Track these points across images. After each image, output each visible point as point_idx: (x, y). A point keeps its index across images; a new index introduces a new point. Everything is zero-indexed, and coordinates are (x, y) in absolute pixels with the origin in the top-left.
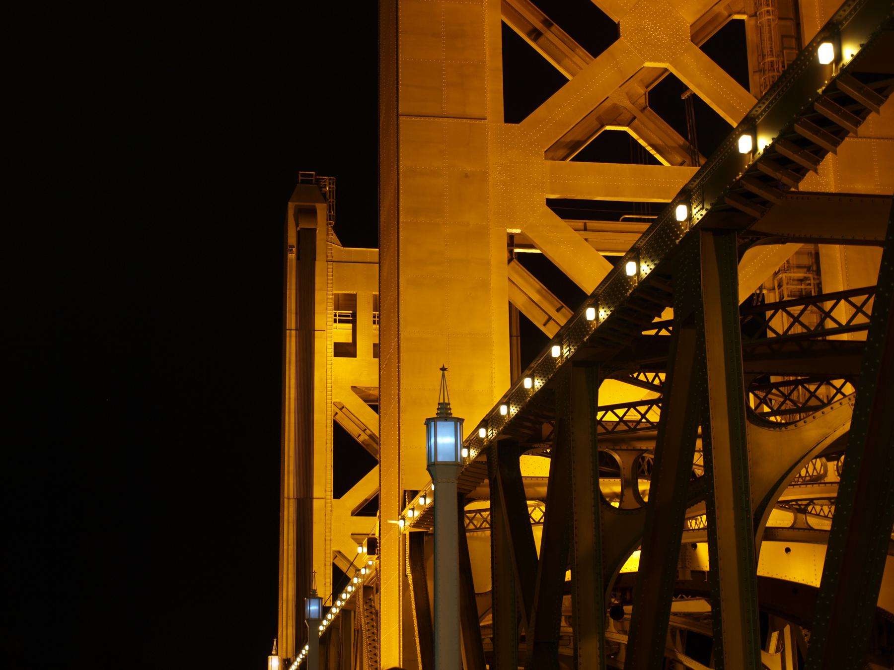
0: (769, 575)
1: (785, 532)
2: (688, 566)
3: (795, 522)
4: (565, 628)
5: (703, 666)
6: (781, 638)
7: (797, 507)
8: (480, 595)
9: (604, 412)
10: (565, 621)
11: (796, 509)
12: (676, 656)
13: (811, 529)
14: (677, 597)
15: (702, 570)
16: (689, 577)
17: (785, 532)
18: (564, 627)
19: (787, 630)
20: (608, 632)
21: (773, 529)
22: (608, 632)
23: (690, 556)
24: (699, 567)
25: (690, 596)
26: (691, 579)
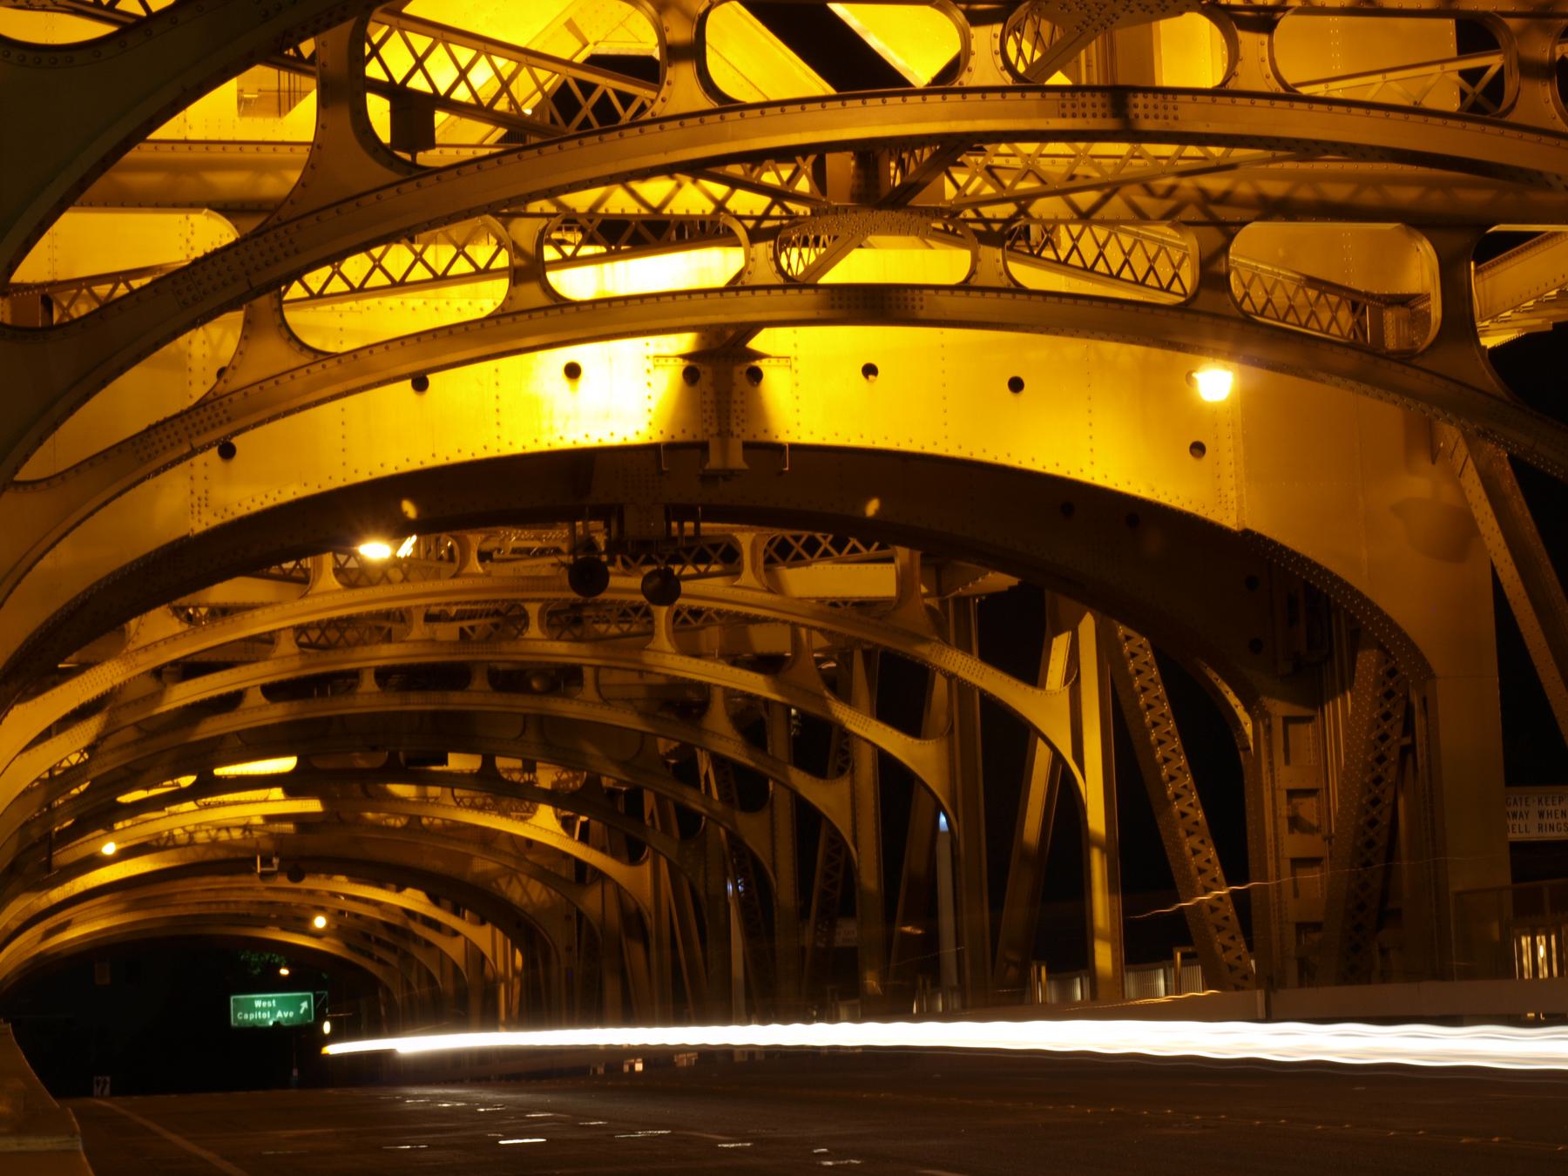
0: (963, 453)
1: (944, 299)
2: (736, 430)
3: (973, 272)
4: (540, 644)
5: (896, 733)
6: (1329, 708)
7: (980, 227)
8: (29, 487)
9: (1034, 60)
10: (541, 626)
11: (976, 232)
12: (828, 711)
13: (1019, 289)
14: (843, 549)
15: (774, 440)
16: (737, 460)
17: (944, 299)
18: (539, 640)
19: (1088, 625)
20: (648, 650)
21: (917, 292)
22: (648, 650)
23: (742, 402)
24: (766, 431)
25: (876, 545)
26: (745, 466)
